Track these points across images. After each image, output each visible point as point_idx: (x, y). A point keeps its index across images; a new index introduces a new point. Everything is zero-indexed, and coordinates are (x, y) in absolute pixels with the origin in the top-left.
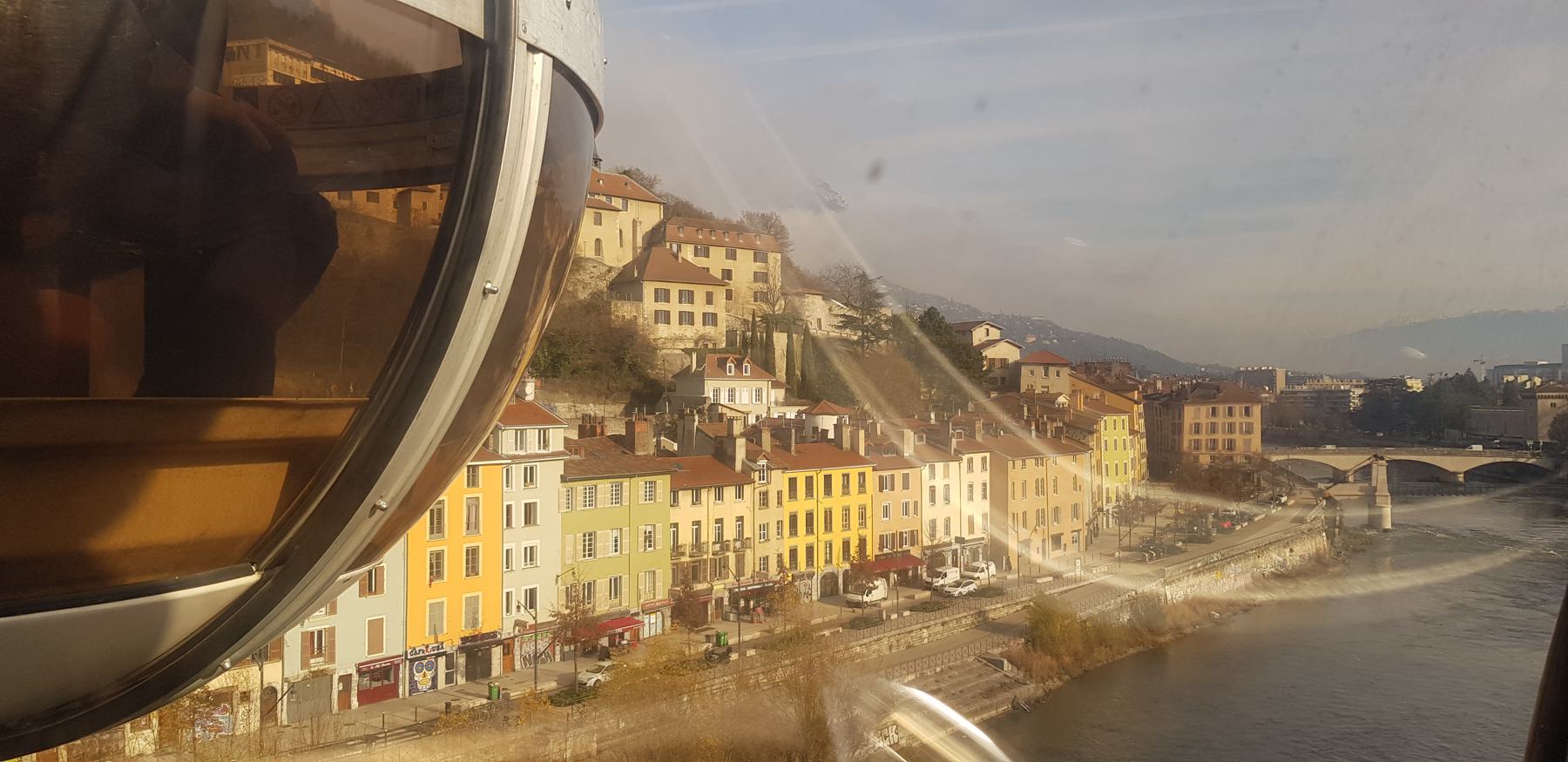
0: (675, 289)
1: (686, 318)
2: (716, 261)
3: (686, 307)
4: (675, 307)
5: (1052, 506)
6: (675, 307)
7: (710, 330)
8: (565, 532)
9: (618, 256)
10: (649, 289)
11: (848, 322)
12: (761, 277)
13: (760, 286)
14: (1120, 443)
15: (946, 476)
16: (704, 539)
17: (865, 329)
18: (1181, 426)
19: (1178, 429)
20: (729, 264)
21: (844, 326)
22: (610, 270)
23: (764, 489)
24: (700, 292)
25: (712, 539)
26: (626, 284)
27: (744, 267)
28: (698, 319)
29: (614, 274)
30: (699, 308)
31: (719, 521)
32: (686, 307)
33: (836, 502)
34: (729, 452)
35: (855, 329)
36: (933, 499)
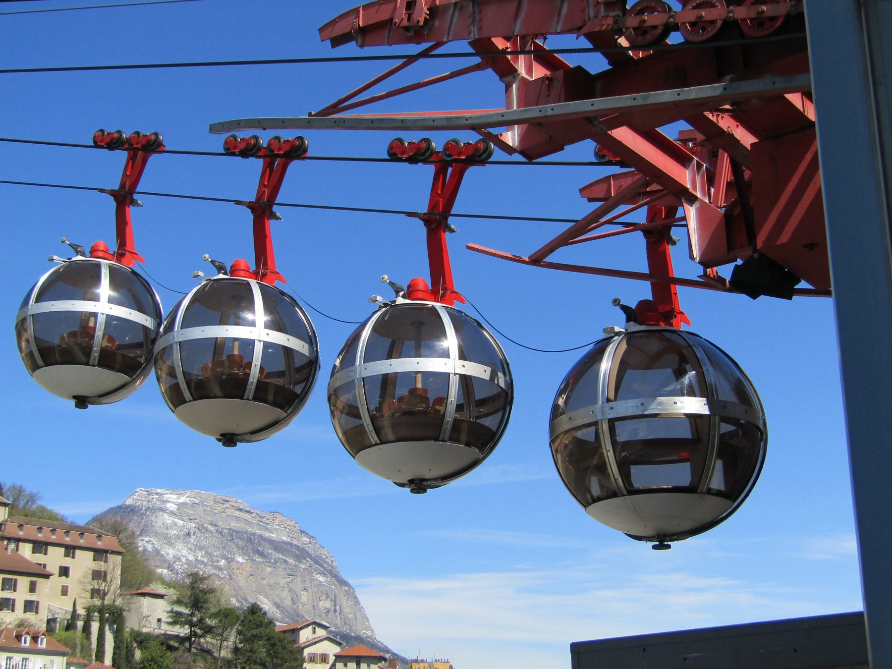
2: (54, 558)
7: (30, 616)
12: (98, 575)
17: (192, 625)
20: (67, 562)
21: (174, 623)
24: (23, 582)
30: (21, 595)
35: (182, 624)
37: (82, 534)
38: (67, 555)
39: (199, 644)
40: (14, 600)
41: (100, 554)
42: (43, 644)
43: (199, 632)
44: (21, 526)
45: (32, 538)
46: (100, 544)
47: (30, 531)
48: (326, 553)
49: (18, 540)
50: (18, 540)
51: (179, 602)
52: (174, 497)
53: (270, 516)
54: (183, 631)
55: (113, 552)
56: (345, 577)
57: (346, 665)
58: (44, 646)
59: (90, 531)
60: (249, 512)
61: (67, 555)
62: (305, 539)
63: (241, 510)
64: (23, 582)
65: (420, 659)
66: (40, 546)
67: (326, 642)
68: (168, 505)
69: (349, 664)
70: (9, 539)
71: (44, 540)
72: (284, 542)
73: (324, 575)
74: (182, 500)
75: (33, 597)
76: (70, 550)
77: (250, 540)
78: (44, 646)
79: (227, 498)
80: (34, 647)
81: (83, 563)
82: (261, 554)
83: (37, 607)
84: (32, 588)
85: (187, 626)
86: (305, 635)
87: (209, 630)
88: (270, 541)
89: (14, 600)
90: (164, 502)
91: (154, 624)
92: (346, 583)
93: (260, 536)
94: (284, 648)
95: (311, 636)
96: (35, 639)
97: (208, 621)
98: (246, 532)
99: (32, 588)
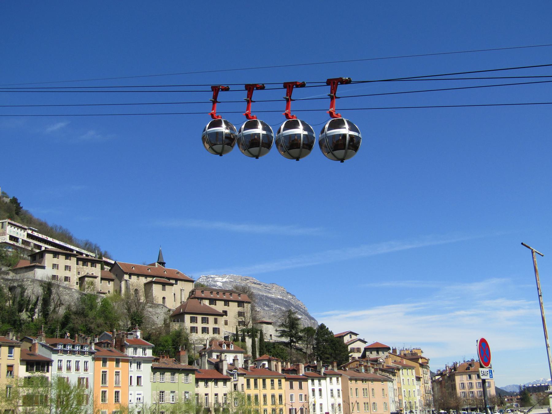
0: (199, 318)
1: (205, 330)
2: (220, 307)
3: (205, 325)
4: (199, 325)
5: (372, 402)
6: (199, 325)
7: (216, 335)
8: (152, 390)
9: (173, 305)
10: (187, 318)
11: (283, 334)
12: (240, 314)
13: (241, 319)
14: (411, 381)
15: (320, 384)
16: (210, 401)
17: (291, 336)
18: (455, 385)
19: (454, 387)
20: (226, 308)
21: (282, 336)
22: (169, 310)
23: (235, 383)
24: (211, 319)
25: (213, 402)
26: (178, 316)
27: (233, 309)
28: (211, 331)
29: (171, 312)
30: (211, 325)
31: (216, 395)
32: (205, 325)
33: (269, 392)
34: (221, 367)
35: (286, 336)
36: (314, 395)
37: (231, 294)
38: (225, 305)
39: (295, 346)
40: (197, 327)
41: (240, 303)
42: (232, 348)
43: (294, 340)
44: (202, 292)
45: (208, 297)
46: (240, 299)
47: (207, 294)
48: (300, 303)
49: (202, 299)
50: (202, 299)
51: (282, 325)
52: (221, 279)
53: (270, 286)
54: (285, 340)
55: (246, 302)
56: (312, 315)
57: (371, 353)
58: (233, 349)
59: (235, 292)
60: (259, 284)
61: (225, 305)
62: (290, 297)
63: (255, 283)
64: (211, 319)
65: (168, 375)
66: (213, 301)
67: (358, 342)
68: (218, 283)
69: (373, 352)
70: (198, 298)
71: (214, 298)
72: (279, 299)
73: (301, 315)
74: (224, 280)
75: (216, 326)
76: (227, 302)
77: (261, 299)
78: (233, 349)
79: (248, 278)
80: (228, 349)
81: (233, 309)
82: (268, 306)
83: (219, 331)
84: (216, 322)
85: (289, 338)
86: (346, 339)
87: (300, 338)
88: (272, 299)
89: (197, 327)
90: (215, 282)
91: (269, 338)
92: (313, 319)
93: (266, 296)
94: (340, 346)
95: (350, 340)
96: (228, 346)
97: (300, 334)
98: (259, 295)
99: (216, 322)
